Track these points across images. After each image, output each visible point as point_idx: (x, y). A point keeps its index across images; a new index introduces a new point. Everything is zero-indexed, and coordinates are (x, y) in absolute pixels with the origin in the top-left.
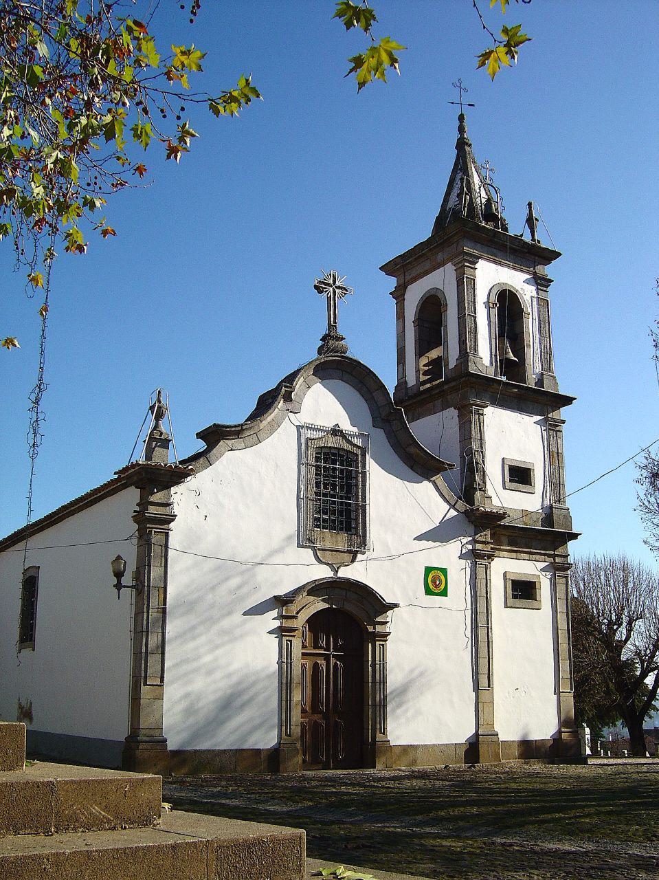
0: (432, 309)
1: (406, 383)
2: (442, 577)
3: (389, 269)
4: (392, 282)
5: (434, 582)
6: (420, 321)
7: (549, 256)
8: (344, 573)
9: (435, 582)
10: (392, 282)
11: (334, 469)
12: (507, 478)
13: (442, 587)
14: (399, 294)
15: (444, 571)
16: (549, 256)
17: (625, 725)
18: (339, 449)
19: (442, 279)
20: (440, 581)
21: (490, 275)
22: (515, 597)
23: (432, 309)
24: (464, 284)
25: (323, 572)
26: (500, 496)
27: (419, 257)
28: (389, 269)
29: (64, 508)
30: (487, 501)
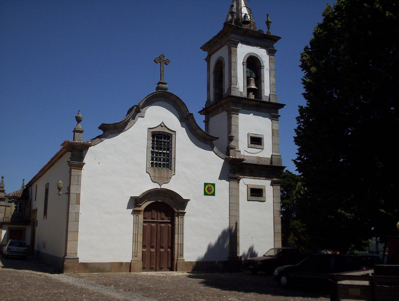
0: (220, 65)
1: (210, 100)
2: (213, 188)
3: (204, 48)
4: (205, 54)
5: (208, 189)
6: (215, 72)
7: (275, 39)
8: (164, 186)
9: (209, 190)
10: (205, 54)
11: (161, 142)
12: (249, 143)
13: (212, 192)
14: (208, 60)
15: (214, 185)
16: (275, 39)
17: (371, 238)
18: (163, 132)
19: (222, 52)
20: (211, 189)
21: (243, 51)
22: (251, 195)
23: (220, 65)
24: (231, 54)
25: (156, 186)
26: (244, 150)
27: (215, 43)
28: (204, 48)
29: (52, 159)
30: (237, 153)
